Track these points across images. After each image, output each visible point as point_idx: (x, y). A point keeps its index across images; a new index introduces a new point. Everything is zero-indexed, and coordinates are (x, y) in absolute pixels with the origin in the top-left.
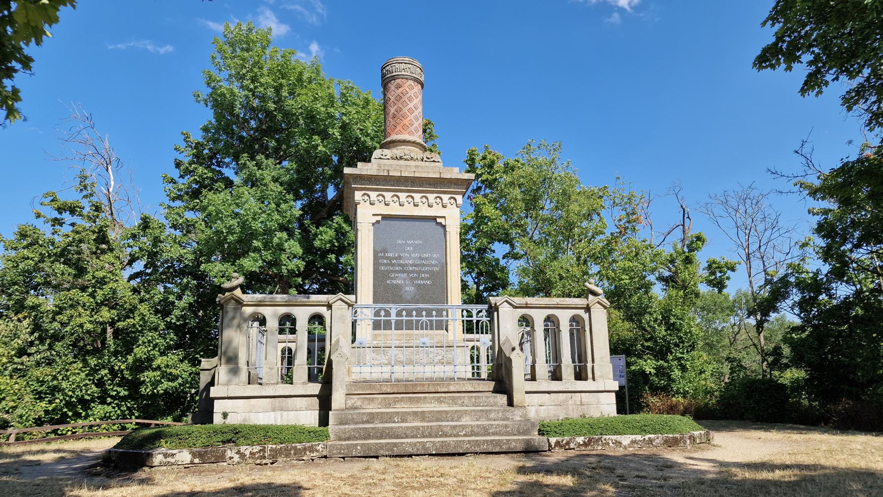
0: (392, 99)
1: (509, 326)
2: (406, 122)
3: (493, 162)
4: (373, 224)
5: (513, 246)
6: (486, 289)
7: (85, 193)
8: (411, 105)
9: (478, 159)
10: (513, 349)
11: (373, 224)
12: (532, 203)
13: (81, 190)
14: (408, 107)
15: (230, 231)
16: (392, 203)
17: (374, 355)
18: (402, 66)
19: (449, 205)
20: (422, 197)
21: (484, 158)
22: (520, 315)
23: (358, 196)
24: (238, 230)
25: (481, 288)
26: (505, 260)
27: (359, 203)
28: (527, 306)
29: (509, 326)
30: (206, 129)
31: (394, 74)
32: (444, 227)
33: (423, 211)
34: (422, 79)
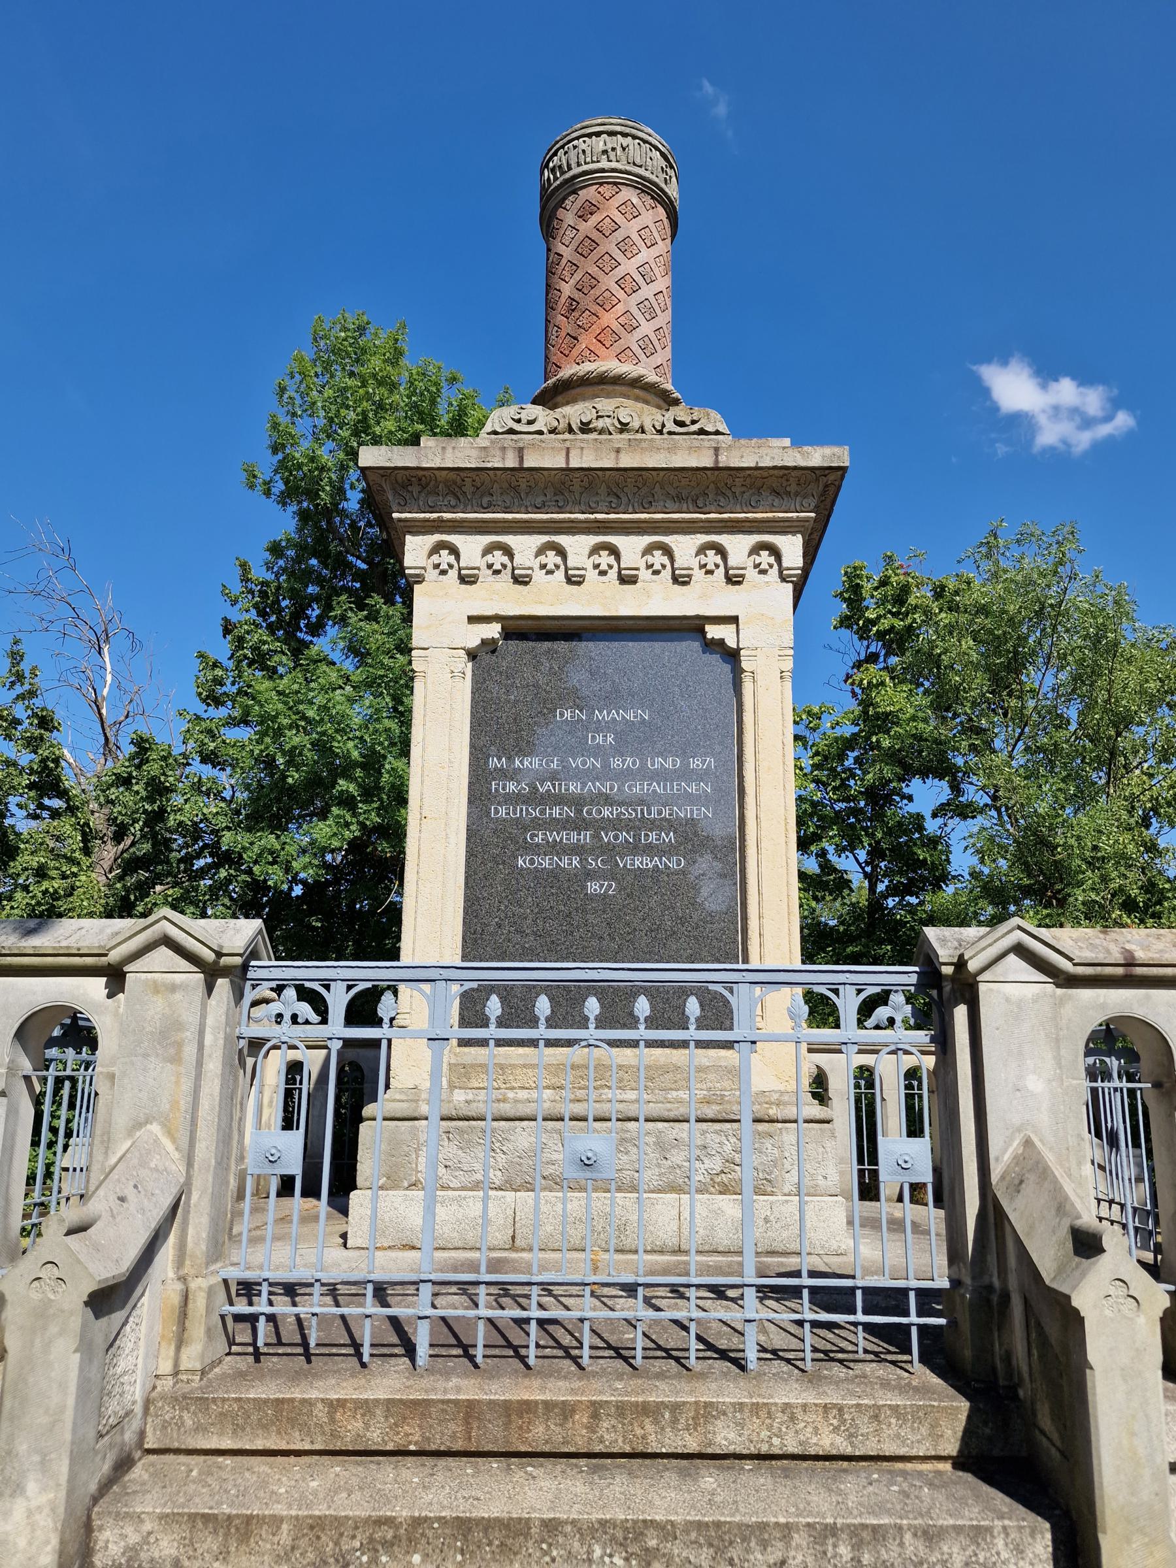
0: (567, 252)
1: (1035, 1084)
2: (609, 319)
3: (905, 590)
4: (472, 655)
5: (956, 788)
6: (893, 891)
7: (19, 690)
8: (629, 266)
9: (867, 586)
10: (1087, 1245)
11: (472, 655)
12: (1006, 671)
13: (13, 683)
14: (620, 272)
15: (293, 756)
16: (538, 576)
17: (450, 1150)
18: (599, 144)
19: (751, 574)
20: (648, 550)
21: (884, 583)
22: (1094, 1020)
23: (416, 551)
24: (310, 755)
25: (881, 887)
26: (939, 821)
27: (420, 579)
28: (1130, 976)
29: (1035, 1084)
30: (276, 549)
31: (576, 170)
32: (732, 656)
33: (656, 599)
34: (673, 190)
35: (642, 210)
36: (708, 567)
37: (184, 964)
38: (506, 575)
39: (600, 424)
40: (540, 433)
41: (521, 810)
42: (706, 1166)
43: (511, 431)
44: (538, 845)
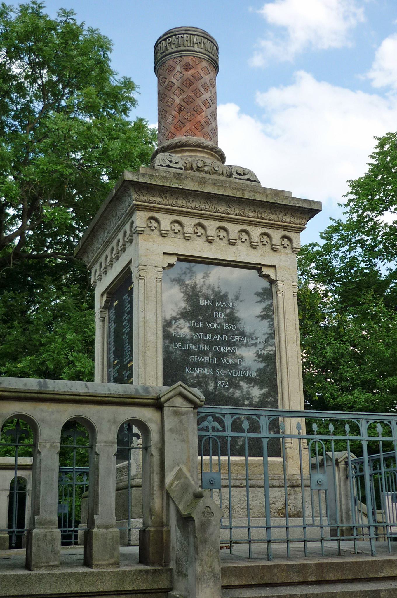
16: (239, 242)
35: (210, 71)
36: (198, 234)
37: (189, 405)
38: (225, 240)
39: (206, 169)
40: (181, 169)
41: (186, 345)
42: (277, 506)
43: (168, 166)
44: (194, 362)
